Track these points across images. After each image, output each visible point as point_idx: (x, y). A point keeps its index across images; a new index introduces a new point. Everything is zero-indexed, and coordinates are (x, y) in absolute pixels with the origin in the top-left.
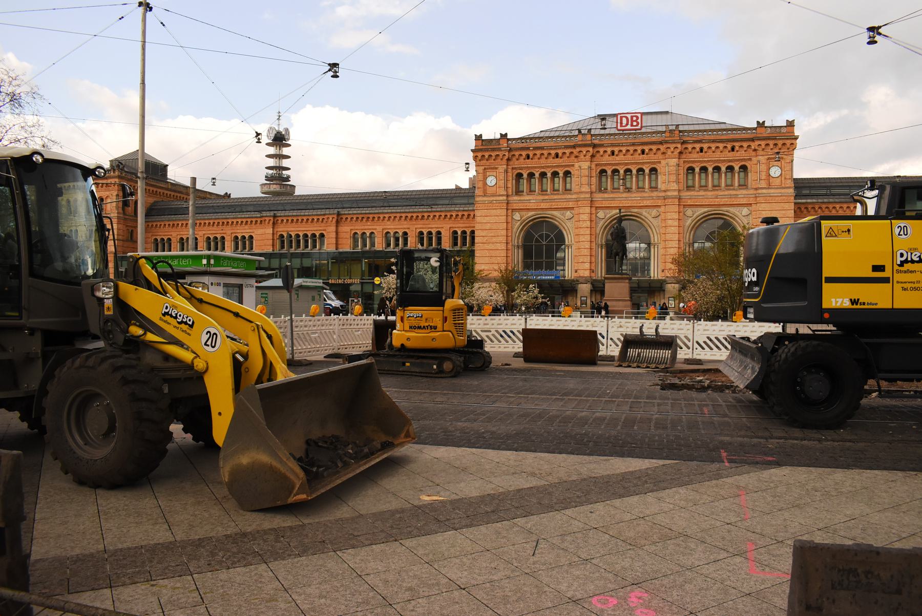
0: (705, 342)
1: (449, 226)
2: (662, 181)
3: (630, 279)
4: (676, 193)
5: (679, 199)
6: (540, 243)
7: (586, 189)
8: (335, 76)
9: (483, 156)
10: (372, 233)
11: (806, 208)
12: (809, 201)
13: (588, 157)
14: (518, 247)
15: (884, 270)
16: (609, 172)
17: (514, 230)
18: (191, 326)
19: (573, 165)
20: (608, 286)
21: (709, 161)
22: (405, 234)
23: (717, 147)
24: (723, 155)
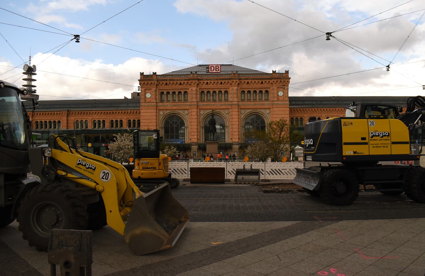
0: (270, 172)
1: (126, 117)
2: (230, 97)
3: (218, 143)
4: (237, 103)
5: (238, 105)
6: (173, 125)
7: (194, 100)
8: (78, 41)
9: (144, 83)
10: (86, 121)
11: (294, 110)
12: (295, 107)
13: (196, 85)
15: (365, 140)
16: (206, 92)
17: (160, 120)
18: (94, 170)
19: (188, 89)
20: (208, 147)
21: (251, 88)
22: (104, 121)
23: (255, 82)
24: (209, 86)
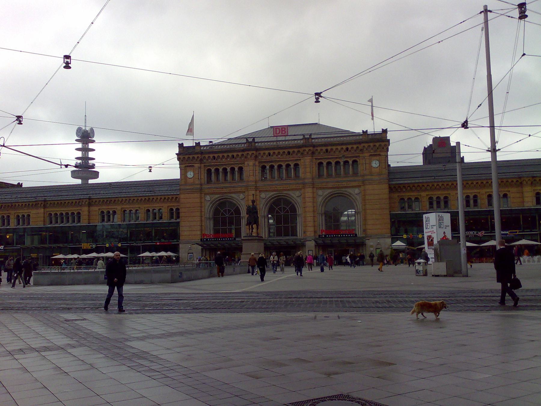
5: (313, 184)
14: (209, 218)
24: (273, 158)
